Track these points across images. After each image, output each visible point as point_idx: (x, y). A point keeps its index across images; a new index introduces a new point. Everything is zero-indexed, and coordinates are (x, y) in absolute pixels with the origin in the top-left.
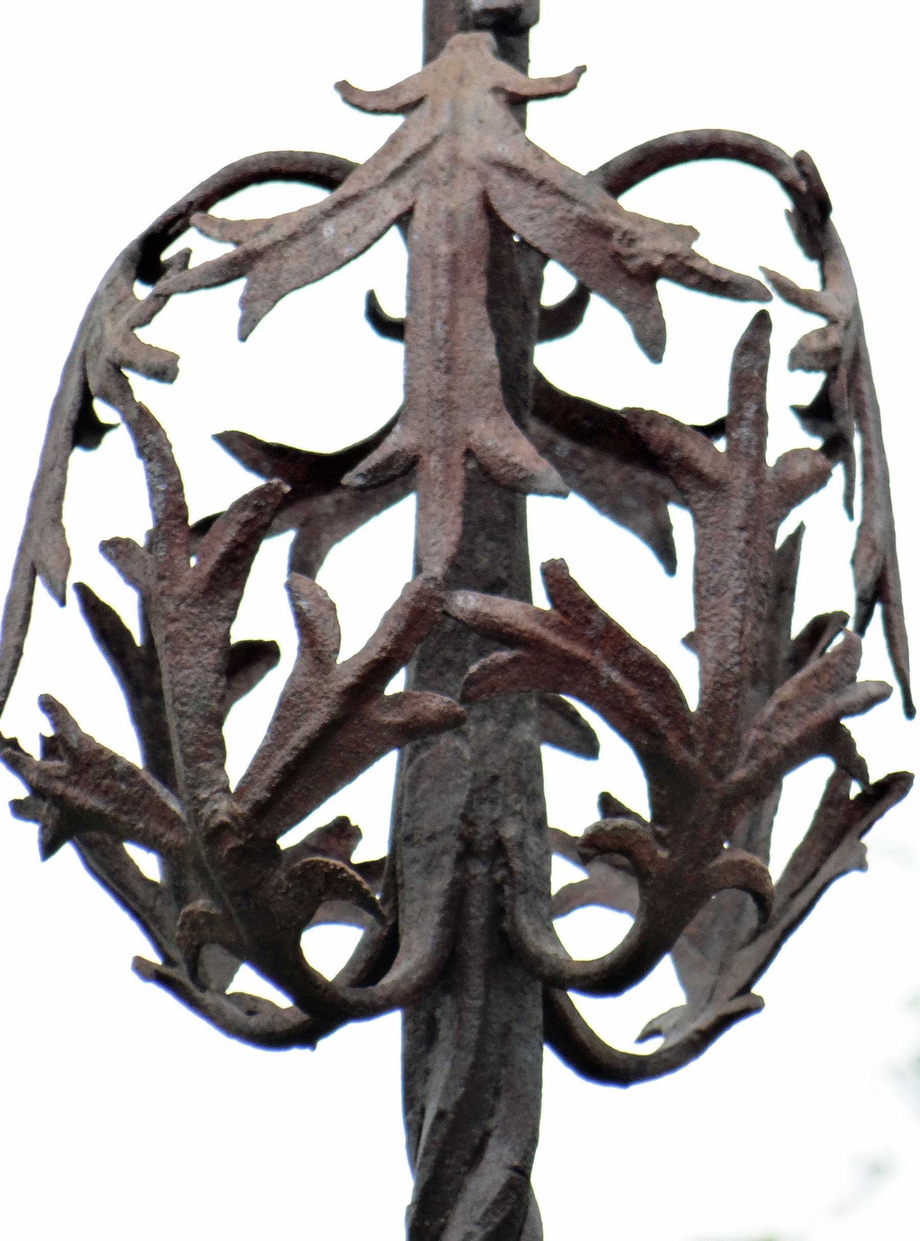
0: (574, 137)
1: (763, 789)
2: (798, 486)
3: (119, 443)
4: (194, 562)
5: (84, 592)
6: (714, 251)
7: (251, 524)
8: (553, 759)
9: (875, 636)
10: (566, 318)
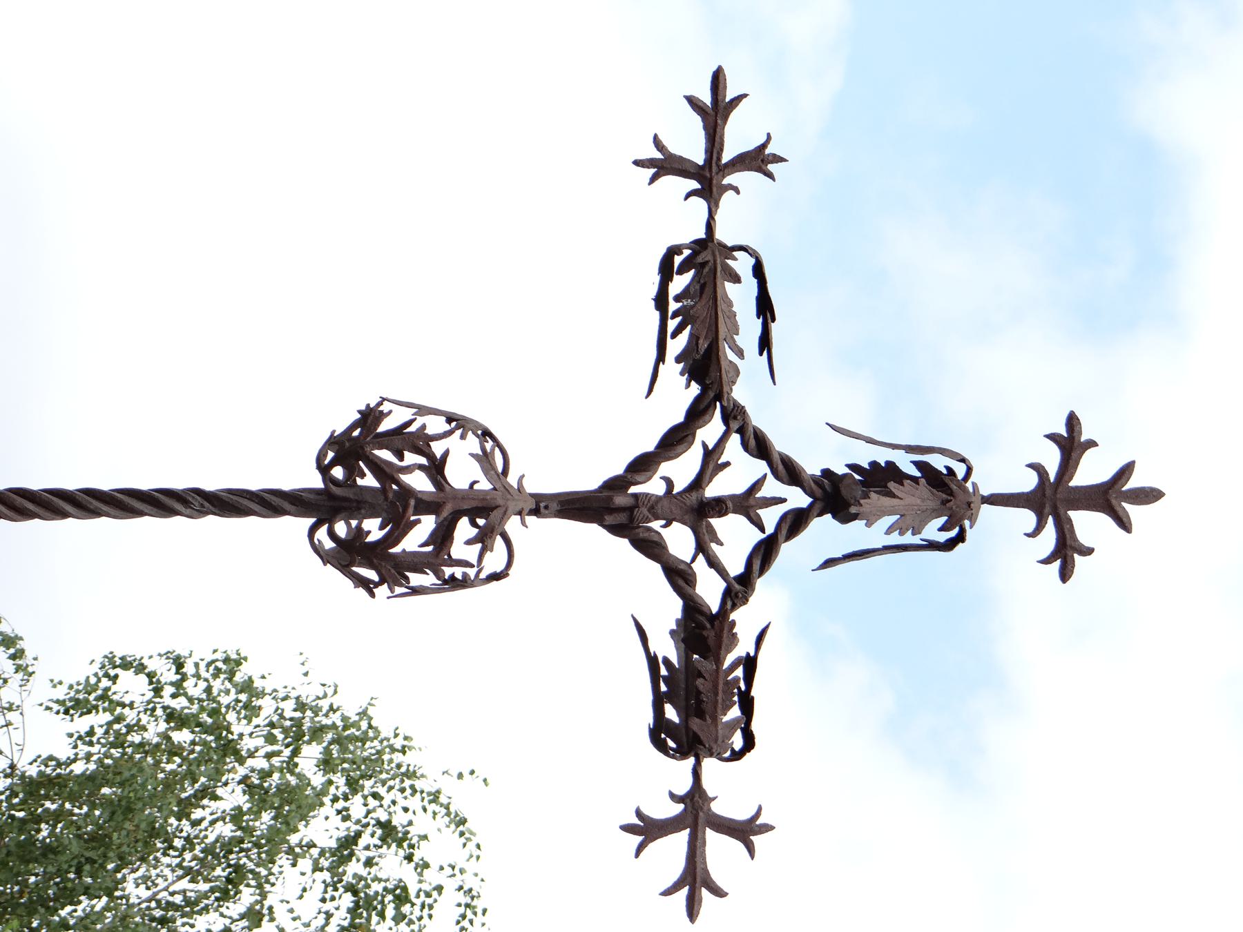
0: (513, 525)
1: (371, 566)
2: (438, 574)
3: (447, 427)
4: (420, 443)
5: (414, 420)
6: (488, 555)
7: (430, 456)
8: (378, 521)
9: (404, 590)
10: (474, 524)
